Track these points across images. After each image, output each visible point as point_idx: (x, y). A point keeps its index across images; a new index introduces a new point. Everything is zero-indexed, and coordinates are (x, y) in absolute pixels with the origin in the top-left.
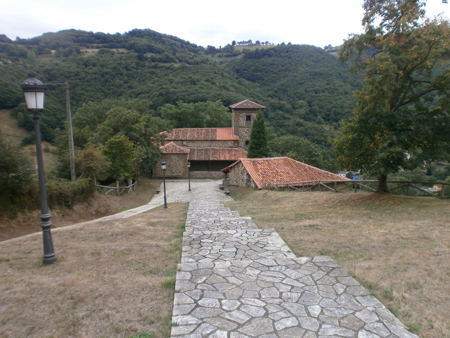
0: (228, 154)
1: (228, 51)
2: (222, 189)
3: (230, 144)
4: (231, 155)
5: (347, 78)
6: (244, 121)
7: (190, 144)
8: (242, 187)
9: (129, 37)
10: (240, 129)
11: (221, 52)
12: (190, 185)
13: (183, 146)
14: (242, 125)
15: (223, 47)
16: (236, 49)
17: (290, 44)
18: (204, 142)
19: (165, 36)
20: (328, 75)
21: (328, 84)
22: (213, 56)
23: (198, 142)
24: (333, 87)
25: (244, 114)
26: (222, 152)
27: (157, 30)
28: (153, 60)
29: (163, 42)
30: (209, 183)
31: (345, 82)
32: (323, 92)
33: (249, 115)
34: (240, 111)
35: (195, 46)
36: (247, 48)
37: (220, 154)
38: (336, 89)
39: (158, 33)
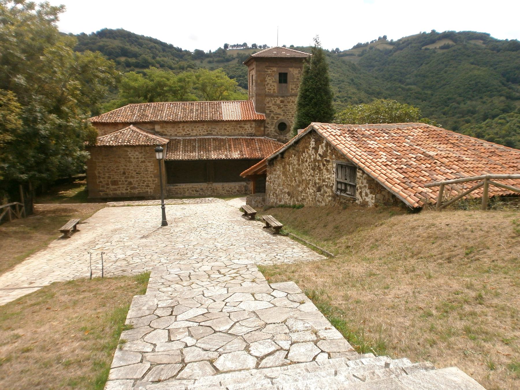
0: (247, 146)
1: (219, 56)
2: (252, 217)
3: (249, 128)
5: (361, 84)
6: (275, 84)
7: (170, 130)
9: (98, 38)
10: (268, 99)
12: (163, 209)
14: (272, 92)
15: (213, 50)
16: (228, 54)
18: (198, 125)
19: (142, 37)
20: (339, 81)
21: (340, 92)
22: (202, 62)
23: (186, 125)
24: (346, 95)
25: (275, 69)
26: (235, 145)
27: (132, 32)
29: (141, 45)
30: (213, 204)
31: (358, 89)
33: (283, 71)
34: (267, 64)
35: (180, 50)
36: (242, 52)
37: (230, 147)
38: (349, 98)
39: (134, 34)
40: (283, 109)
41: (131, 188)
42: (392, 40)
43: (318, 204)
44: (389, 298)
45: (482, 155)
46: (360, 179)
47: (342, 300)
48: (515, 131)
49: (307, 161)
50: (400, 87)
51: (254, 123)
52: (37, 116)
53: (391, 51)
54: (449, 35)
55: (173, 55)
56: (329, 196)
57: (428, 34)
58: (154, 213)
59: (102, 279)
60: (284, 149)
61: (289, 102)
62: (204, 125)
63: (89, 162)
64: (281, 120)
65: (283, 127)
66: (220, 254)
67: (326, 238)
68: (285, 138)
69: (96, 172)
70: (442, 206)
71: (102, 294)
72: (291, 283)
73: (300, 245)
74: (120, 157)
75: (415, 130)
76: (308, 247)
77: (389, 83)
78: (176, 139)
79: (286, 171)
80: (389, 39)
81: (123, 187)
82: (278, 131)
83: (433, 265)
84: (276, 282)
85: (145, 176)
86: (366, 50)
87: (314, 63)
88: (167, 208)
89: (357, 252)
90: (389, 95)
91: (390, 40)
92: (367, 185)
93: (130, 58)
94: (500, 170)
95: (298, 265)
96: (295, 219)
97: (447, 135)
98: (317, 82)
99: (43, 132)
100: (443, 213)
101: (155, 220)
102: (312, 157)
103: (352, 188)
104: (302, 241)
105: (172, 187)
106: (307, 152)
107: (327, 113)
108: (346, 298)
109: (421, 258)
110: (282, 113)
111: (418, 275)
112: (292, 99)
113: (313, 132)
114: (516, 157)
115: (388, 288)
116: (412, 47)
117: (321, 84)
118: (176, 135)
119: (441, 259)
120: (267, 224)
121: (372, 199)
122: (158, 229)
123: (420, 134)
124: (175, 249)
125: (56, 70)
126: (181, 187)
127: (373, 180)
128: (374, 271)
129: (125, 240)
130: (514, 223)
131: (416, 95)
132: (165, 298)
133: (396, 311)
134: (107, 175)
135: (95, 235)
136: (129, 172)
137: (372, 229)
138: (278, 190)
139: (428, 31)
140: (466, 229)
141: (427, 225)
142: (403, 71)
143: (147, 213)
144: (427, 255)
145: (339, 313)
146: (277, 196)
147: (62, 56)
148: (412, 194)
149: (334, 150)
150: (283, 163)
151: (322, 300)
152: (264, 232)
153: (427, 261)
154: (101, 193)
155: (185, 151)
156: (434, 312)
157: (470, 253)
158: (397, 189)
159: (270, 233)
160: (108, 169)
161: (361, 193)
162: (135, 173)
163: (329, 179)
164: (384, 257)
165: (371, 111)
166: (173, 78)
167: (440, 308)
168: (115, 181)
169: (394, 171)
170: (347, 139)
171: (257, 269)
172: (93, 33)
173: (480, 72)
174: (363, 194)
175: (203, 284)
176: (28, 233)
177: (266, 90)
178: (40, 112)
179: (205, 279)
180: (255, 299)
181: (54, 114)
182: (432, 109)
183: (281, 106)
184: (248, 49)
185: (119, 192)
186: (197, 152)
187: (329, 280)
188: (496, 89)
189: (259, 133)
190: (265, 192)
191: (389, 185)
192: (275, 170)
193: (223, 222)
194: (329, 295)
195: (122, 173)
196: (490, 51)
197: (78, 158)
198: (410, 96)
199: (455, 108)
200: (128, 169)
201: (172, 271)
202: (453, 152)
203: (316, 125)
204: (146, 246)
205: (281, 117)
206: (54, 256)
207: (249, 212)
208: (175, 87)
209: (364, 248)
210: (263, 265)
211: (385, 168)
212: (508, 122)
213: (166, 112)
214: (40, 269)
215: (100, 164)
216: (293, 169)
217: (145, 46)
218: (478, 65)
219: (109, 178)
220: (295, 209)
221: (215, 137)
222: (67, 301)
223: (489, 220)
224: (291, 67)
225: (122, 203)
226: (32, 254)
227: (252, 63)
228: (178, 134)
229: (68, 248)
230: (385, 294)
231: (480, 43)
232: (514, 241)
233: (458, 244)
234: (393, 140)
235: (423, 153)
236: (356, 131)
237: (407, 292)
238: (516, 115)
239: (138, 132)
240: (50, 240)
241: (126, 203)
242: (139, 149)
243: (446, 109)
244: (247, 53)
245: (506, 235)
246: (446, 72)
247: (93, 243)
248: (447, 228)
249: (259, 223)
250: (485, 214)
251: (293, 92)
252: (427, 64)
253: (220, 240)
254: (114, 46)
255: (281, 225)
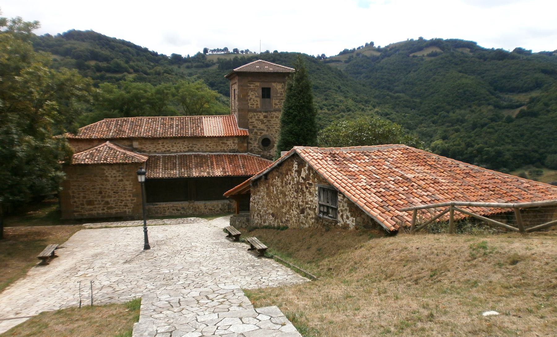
0: (230, 163)
1: (199, 62)
2: (237, 239)
3: (231, 144)
4: (237, 167)
5: (348, 92)
6: (258, 99)
8: (300, 229)
10: (251, 114)
11: (190, 62)
12: (146, 232)
13: (133, 150)
16: (208, 59)
17: (276, 52)
18: (178, 141)
19: (114, 40)
20: (325, 88)
21: (326, 99)
22: (179, 67)
23: (166, 141)
24: (333, 103)
25: (258, 84)
26: (217, 161)
28: (99, 69)
29: (112, 48)
30: (195, 225)
31: (346, 97)
32: (321, 109)
33: (266, 86)
34: (250, 79)
35: (155, 54)
36: (223, 57)
37: (212, 164)
40: (266, 124)
41: (108, 208)
42: (379, 47)
43: (302, 225)
44: (358, 319)
45: (458, 176)
46: (341, 202)
47: (318, 321)
48: (503, 140)
49: (290, 183)
50: (388, 95)
51: (236, 139)
52: (13, 137)
53: (378, 58)
54: (437, 43)
55: (148, 59)
56: (312, 218)
57: (416, 41)
58: (134, 235)
59: (91, 307)
60: (267, 170)
61: (272, 117)
62: (184, 141)
63: (66, 184)
64: (265, 135)
65: (266, 142)
66: (206, 278)
67: (309, 260)
68: (268, 154)
69: (70, 192)
70: (416, 229)
71: (96, 322)
72: (274, 307)
73: (284, 268)
74: (96, 176)
75: (394, 152)
76: (291, 269)
77: (377, 91)
78: (155, 156)
79: (270, 192)
80: (376, 45)
81: (100, 207)
82: (261, 146)
83: (403, 286)
84: (261, 306)
85: (122, 195)
86: (352, 57)
87: (297, 80)
88: (149, 228)
89: (338, 274)
90: (377, 103)
91: (377, 47)
92: (348, 208)
93: (100, 62)
94: (473, 191)
95: (282, 288)
96: (280, 241)
97: (425, 157)
98: (300, 100)
99: (20, 154)
100: (416, 236)
101: (136, 243)
102: (295, 179)
103: (334, 211)
104: (286, 263)
105: (152, 206)
106: (291, 175)
107: (311, 131)
108: (322, 319)
109: (394, 280)
110: (266, 129)
111: (388, 296)
112: (276, 114)
113: (296, 155)
114: (489, 178)
115: (358, 309)
116: (399, 54)
117: (304, 102)
118: (155, 152)
119: (410, 281)
120: (252, 246)
121: (353, 222)
122: (141, 253)
123: (399, 156)
124: (160, 274)
125: (33, 90)
126: (161, 206)
127: (353, 204)
128: (352, 293)
129: (107, 265)
130: (471, 248)
131: (404, 103)
132: (163, 324)
133: (362, 329)
134: (82, 195)
135: (74, 261)
136: (106, 191)
137: (352, 252)
138: (262, 211)
139: (416, 38)
140: (433, 253)
141: (400, 249)
142: (391, 78)
143: (128, 235)
144: (399, 277)
145: (314, 332)
146: (261, 217)
147: (40, 76)
148: (389, 218)
149: (316, 174)
150: (267, 185)
151: (301, 322)
152: (249, 255)
153: (398, 283)
154: (76, 214)
155: (165, 169)
156: (392, 329)
157: (434, 275)
158: (375, 213)
159: (255, 255)
160: (83, 189)
161: (342, 216)
162: (112, 192)
163: (312, 201)
164: (362, 279)
165: (354, 128)
166: (149, 89)
167: (397, 326)
168: (90, 201)
169: (373, 194)
170: (329, 162)
171: (243, 294)
172: (59, 35)
173: (468, 80)
174: (345, 217)
175: (193, 309)
176: (4, 261)
177: (249, 105)
178: (16, 134)
179: (194, 304)
180: (243, 323)
181: (30, 135)
182: (421, 118)
183: (265, 121)
184: (230, 54)
185: (95, 212)
186: (177, 169)
187: (310, 303)
188: (484, 97)
189: (242, 149)
190: (249, 210)
191: (368, 209)
192: (259, 191)
193: (207, 244)
194: (308, 317)
195: (98, 192)
196: (477, 60)
197: (53, 179)
198: (398, 104)
199: (444, 117)
200: (105, 188)
201: (163, 297)
202: (430, 174)
203: (298, 149)
204: (130, 271)
205: (264, 133)
206: (35, 285)
207: (233, 233)
208: (153, 99)
209: (344, 270)
210: (248, 288)
211: (364, 192)
212: (496, 131)
213: (144, 127)
214: (24, 298)
215: (75, 183)
216: (277, 190)
217: (117, 49)
218: (466, 73)
219: (84, 197)
220: (279, 231)
221: (196, 153)
222: (63, 330)
223: (452, 245)
224: (275, 82)
225: (99, 225)
226: (12, 282)
227: (234, 77)
228: (157, 151)
229: (50, 275)
230: (355, 315)
231: (467, 51)
232: (469, 264)
233: (424, 267)
234: (373, 163)
235: (402, 176)
236: (338, 154)
237: (373, 313)
238: (504, 124)
239: (115, 150)
240: (29, 267)
241: (104, 224)
242: (116, 167)
243: (436, 117)
244: (228, 58)
245: (464, 259)
246: (434, 80)
247: (74, 270)
248: (417, 252)
249: (244, 244)
250: (450, 238)
251: (277, 107)
252: (415, 71)
253: (205, 264)
254: (82, 48)
255: (266, 247)
